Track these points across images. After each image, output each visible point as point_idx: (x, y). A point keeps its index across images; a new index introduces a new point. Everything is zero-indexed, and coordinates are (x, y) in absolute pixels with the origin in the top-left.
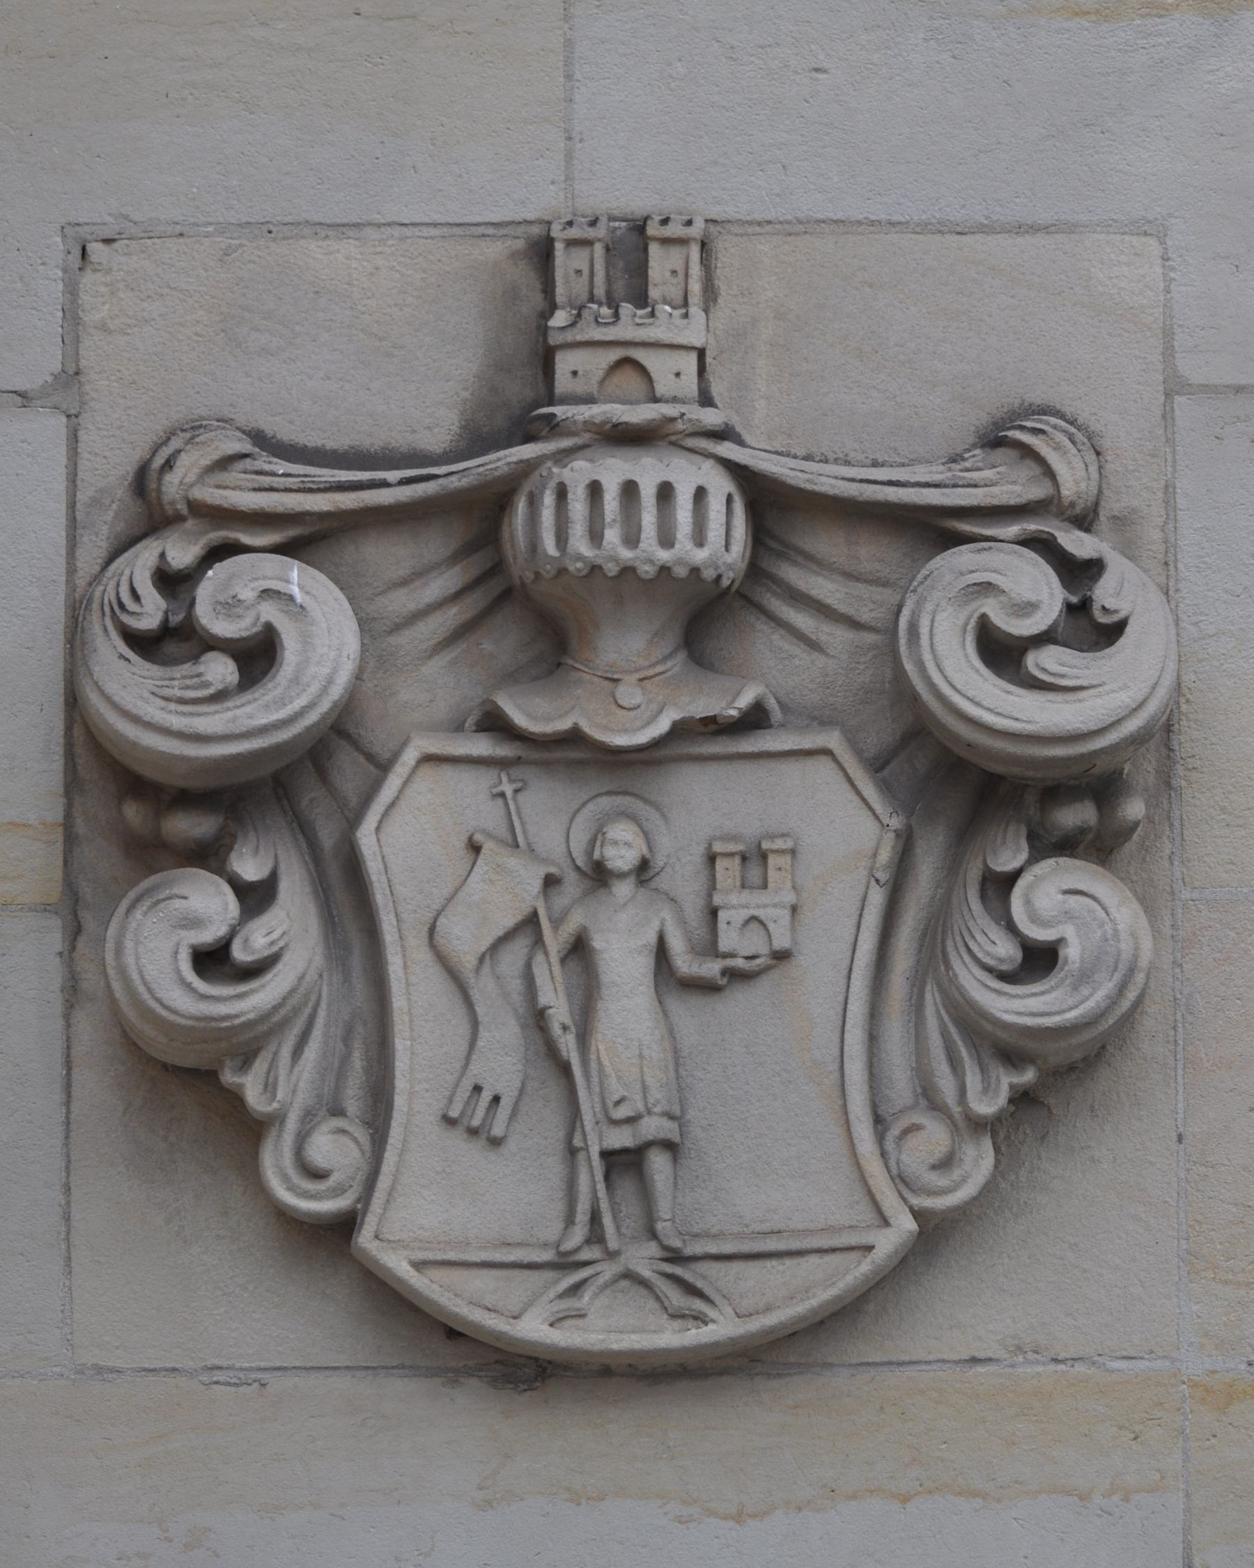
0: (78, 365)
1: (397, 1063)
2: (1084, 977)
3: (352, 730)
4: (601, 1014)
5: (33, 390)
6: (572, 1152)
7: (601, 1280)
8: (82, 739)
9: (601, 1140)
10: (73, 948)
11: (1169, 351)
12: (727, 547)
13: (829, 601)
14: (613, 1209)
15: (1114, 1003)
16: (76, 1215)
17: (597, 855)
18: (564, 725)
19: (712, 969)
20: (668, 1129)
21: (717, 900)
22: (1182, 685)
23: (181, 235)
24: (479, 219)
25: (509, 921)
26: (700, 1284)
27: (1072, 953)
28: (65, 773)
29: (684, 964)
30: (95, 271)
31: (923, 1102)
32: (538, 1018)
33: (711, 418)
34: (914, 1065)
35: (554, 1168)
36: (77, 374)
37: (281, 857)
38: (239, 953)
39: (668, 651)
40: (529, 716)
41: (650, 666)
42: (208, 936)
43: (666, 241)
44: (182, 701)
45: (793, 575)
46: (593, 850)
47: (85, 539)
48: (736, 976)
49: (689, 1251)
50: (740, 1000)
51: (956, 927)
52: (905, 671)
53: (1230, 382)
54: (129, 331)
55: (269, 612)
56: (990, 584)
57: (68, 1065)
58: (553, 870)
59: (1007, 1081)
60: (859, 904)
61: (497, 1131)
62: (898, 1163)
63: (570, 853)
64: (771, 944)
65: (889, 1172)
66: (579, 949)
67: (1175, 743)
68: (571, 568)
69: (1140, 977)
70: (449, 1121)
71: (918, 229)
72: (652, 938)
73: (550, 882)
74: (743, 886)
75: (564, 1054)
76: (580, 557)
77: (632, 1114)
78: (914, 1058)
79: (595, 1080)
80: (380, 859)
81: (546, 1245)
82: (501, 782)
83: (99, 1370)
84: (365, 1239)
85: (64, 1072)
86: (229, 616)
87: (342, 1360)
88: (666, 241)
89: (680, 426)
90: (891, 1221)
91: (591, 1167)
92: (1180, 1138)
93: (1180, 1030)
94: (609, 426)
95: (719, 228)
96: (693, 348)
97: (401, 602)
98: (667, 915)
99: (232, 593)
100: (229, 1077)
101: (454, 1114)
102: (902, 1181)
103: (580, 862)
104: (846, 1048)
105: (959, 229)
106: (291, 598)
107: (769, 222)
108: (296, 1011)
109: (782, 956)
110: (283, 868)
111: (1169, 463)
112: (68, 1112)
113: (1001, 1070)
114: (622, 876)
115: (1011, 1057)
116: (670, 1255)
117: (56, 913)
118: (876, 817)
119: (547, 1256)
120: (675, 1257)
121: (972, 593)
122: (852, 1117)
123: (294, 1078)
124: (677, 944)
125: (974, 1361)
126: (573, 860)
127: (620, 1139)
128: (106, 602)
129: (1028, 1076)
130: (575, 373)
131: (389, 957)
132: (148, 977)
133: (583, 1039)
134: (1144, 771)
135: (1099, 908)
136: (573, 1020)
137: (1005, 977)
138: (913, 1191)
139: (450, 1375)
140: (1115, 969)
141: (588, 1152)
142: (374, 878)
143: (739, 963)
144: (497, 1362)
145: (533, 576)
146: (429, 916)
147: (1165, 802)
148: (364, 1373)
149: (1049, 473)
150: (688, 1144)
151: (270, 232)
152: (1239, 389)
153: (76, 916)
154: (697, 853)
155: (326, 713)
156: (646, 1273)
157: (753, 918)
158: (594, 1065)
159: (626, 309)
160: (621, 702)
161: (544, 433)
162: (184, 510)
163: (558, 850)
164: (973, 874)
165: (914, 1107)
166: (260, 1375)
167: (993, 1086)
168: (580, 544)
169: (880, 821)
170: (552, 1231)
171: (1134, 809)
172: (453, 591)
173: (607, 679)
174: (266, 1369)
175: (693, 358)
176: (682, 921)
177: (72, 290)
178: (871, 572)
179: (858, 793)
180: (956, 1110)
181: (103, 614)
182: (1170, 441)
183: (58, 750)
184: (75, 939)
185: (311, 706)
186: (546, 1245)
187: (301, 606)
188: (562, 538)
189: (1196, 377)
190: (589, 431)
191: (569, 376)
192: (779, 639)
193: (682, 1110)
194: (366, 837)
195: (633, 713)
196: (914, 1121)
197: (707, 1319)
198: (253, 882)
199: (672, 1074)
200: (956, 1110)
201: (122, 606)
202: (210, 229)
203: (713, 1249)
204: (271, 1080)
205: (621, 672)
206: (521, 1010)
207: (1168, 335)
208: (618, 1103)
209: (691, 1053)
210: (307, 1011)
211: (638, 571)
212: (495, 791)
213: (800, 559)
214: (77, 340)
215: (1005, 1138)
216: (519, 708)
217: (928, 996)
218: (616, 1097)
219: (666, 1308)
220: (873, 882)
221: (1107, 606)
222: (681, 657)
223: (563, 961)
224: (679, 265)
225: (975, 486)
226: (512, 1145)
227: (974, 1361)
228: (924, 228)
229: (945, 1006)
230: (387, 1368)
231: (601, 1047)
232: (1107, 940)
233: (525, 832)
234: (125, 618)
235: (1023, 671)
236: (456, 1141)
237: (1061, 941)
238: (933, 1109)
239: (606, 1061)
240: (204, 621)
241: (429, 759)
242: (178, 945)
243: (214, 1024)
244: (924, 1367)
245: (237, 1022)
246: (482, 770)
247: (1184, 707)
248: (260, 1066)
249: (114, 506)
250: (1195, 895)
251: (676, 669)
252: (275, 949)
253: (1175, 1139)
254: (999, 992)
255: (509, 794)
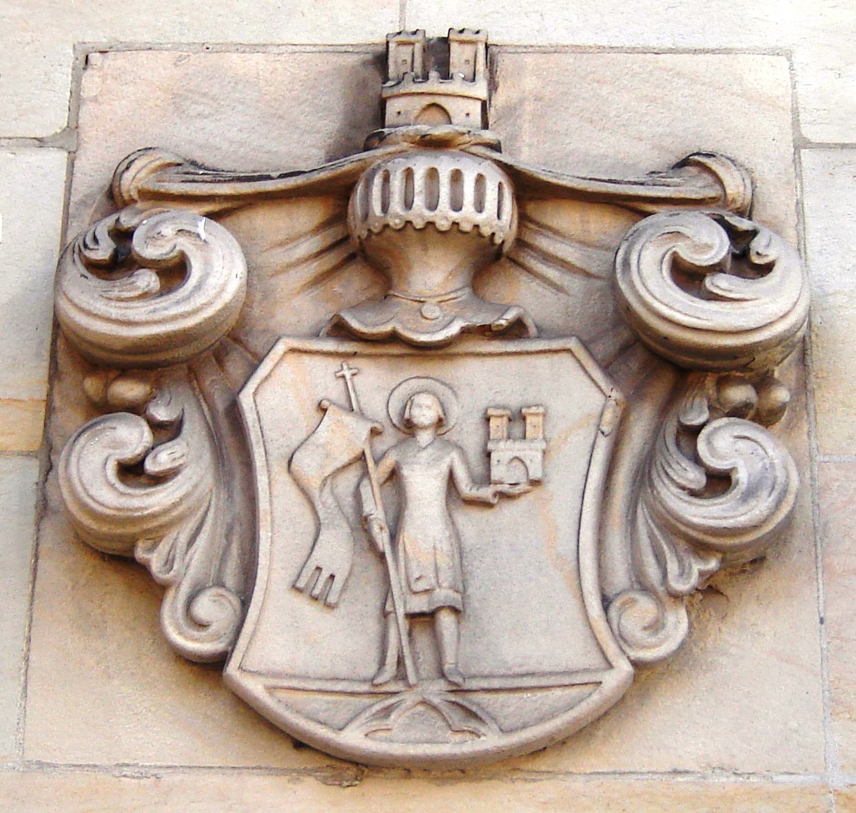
0: (77, 123)
1: (261, 548)
2: (750, 493)
3: (243, 338)
4: (407, 519)
5: (47, 137)
6: (385, 615)
7: (403, 706)
8: (62, 347)
9: (405, 607)
10: (46, 480)
11: (796, 124)
12: (499, 217)
13: (569, 259)
14: (413, 657)
15: (773, 514)
16: (33, 658)
17: (407, 416)
18: (388, 328)
19: (486, 493)
20: (455, 598)
21: (490, 446)
22: (813, 325)
23: (150, 49)
24: (343, 43)
25: (345, 458)
26: (474, 709)
27: (742, 476)
28: (50, 369)
29: (466, 488)
30: (93, 69)
31: (636, 586)
32: (362, 523)
33: (488, 136)
34: (630, 562)
35: (373, 627)
36: (77, 128)
37: (186, 407)
38: (150, 466)
39: (459, 287)
40: (361, 322)
41: (446, 294)
42: (130, 452)
43: (462, 42)
44: (122, 300)
45: (544, 243)
46: (404, 412)
47: (74, 224)
48: (504, 496)
49: (469, 685)
50: (508, 511)
51: (658, 462)
52: (620, 289)
53: (839, 142)
54: (112, 103)
55: (185, 244)
56: (679, 233)
57: (36, 557)
58: (376, 425)
59: (699, 567)
60: (590, 449)
61: (332, 599)
62: (618, 626)
63: (389, 415)
64: (528, 475)
65: (613, 634)
66: (394, 475)
67: (809, 361)
68: (391, 224)
69: (791, 498)
70: (294, 587)
71: (629, 51)
72: (444, 469)
73: (374, 432)
74: (509, 438)
75: (381, 548)
76: (398, 216)
77: (428, 588)
78: (630, 556)
79: (402, 563)
80: (255, 412)
81: (364, 681)
82: (342, 369)
83: (41, 764)
84: (232, 669)
85: (33, 561)
86: (155, 246)
87: (217, 762)
88: (462, 42)
89: (466, 138)
90: (614, 664)
91: (398, 624)
92: (822, 621)
93: (819, 548)
94: (418, 137)
95: (499, 49)
96: (480, 100)
97: (279, 257)
98: (455, 456)
99: (158, 231)
100: (140, 554)
101: (301, 584)
102: (621, 639)
103: (395, 421)
104: (581, 544)
105: (655, 51)
106: (198, 236)
107: (531, 46)
108: (191, 511)
109: (535, 483)
110: (187, 416)
111: (799, 189)
112: (34, 587)
113: (693, 560)
114: (425, 428)
115: (700, 548)
116: (454, 688)
117: (36, 457)
118: (602, 391)
119: (365, 688)
120: (458, 690)
121: (666, 239)
122: (585, 591)
123: (188, 557)
124: (461, 474)
125: (676, 772)
126: (391, 420)
127: (419, 604)
128: (76, 246)
129: (713, 564)
130: (399, 113)
131: (259, 477)
132: (85, 481)
133: (394, 538)
134: (784, 372)
135: (759, 447)
136: (387, 523)
137: (693, 493)
138: (630, 646)
139: (294, 774)
140: (773, 488)
141: (396, 614)
142: (250, 424)
143: (505, 488)
144: (328, 766)
145: (366, 233)
146: (289, 451)
147: (804, 400)
148: (230, 772)
149: (719, 181)
150: (468, 611)
151: (208, 48)
152: (843, 146)
153: (50, 459)
154: (477, 417)
155: (220, 310)
156: (436, 701)
157: (516, 458)
158: (401, 554)
159: (433, 74)
160: (425, 314)
161: (376, 145)
162: (136, 196)
163: (382, 415)
164: (671, 429)
165: (632, 588)
166: (155, 771)
167: (686, 571)
168: (396, 206)
169: (604, 394)
170: (371, 670)
171: (781, 395)
172: (315, 251)
173: (416, 301)
174: (160, 767)
175: (479, 104)
176: (466, 462)
177: (77, 80)
178: (598, 241)
179: (590, 377)
180: (660, 589)
181: (74, 252)
182: (799, 176)
183: (46, 355)
184: (48, 474)
185: (210, 304)
186: (364, 681)
187: (205, 241)
188: (385, 207)
189: (814, 138)
190: (405, 141)
191: (395, 114)
192: (535, 285)
193: (453, 523)
194: (246, 399)
195: (434, 322)
196: (633, 596)
197: (480, 734)
198: (163, 421)
199: (457, 560)
200: (660, 589)
201: (86, 246)
202: (169, 46)
203: (485, 684)
204: (171, 557)
205: (426, 297)
206: (351, 519)
207: (795, 112)
208: (418, 579)
209: (471, 550)
210: (200, 513)
211: (437, 225)
212: (338, 374)
213: (550, 234)
214: (78, 108)
215: (696, 617)
216: (355, 317)
217: (639, 511)
218: (417, 575)
219: (450, 726)
220: (600, 434)
221: (760, 252)
222: (468, 290)
223: (381, 485)
224: (470, 55)
225: (668, 186)
226: (342, 609)
227: (676, 772)
228: (633, 50)
229: (651, 517)
230: (248, 768)
231: (406, 541)
232: (767, 469)
233: (358, 401)
234: (88, 253)
235: (703, 289)
236: (302, 605)
237: (733, 469)
238: (644, 590)
239: (408, 548)
240: (137, 249)
241: (293, 350)
242: (107, 459)
243: (129, 513)
244: (639, 776)
245: (146, 512)
246: (330, 360)
247: (813, 337)
248: (164, 547)
249: (95, 206)
250: (827, 459)
251: (463, 297)
252: (176, 464)
253: (818, 621)
254: (689, 503)
255: (348, 377)
